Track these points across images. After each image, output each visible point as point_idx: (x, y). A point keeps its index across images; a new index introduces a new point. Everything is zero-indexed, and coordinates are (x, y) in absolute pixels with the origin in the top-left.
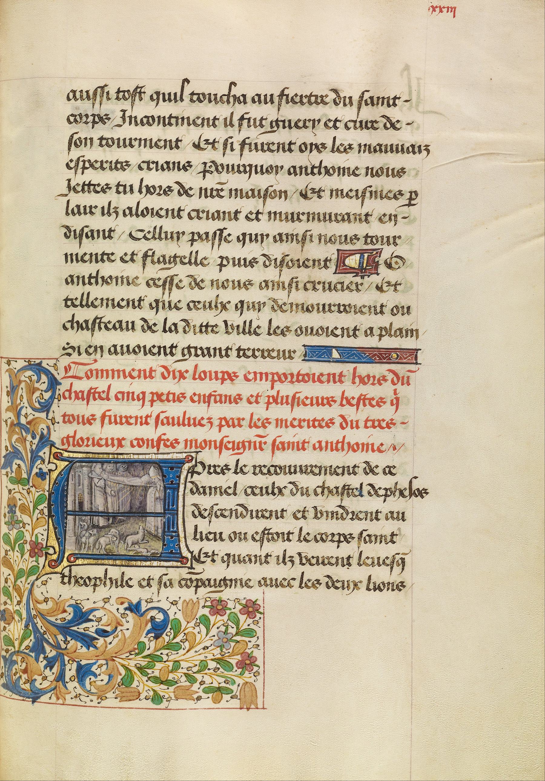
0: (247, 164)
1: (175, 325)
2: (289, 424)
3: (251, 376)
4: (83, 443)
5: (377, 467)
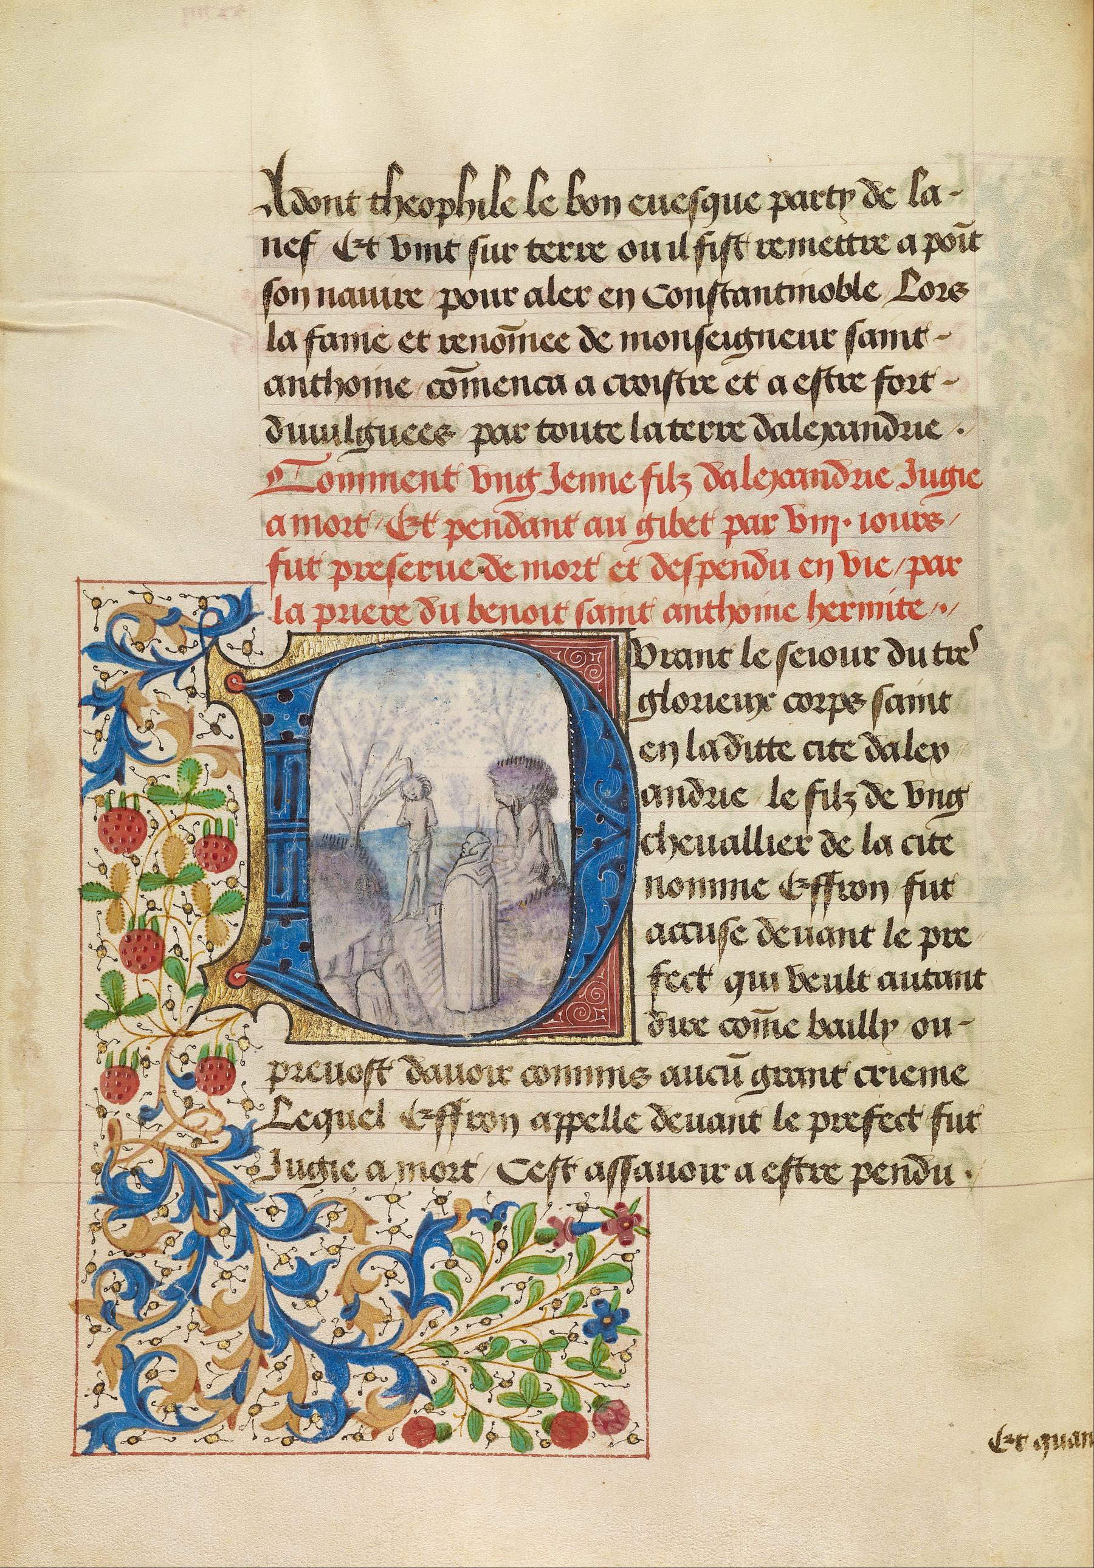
4: (810, 704)
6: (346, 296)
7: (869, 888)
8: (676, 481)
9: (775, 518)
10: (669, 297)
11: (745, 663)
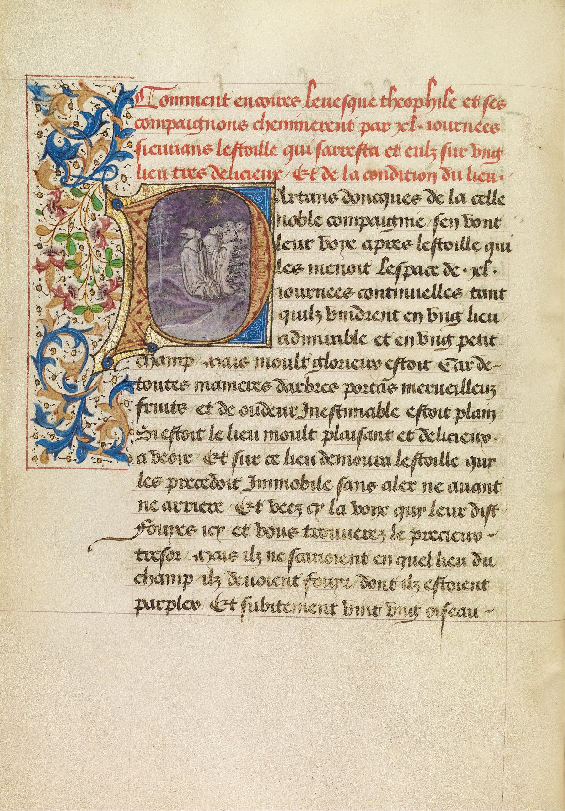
0: (477, 299)
1: (343, 507)
2: (433, 488)
3: (402, 341)
5: (489, 363)
7: (427, 176)
8: (430, 152)
9: (466, 150)
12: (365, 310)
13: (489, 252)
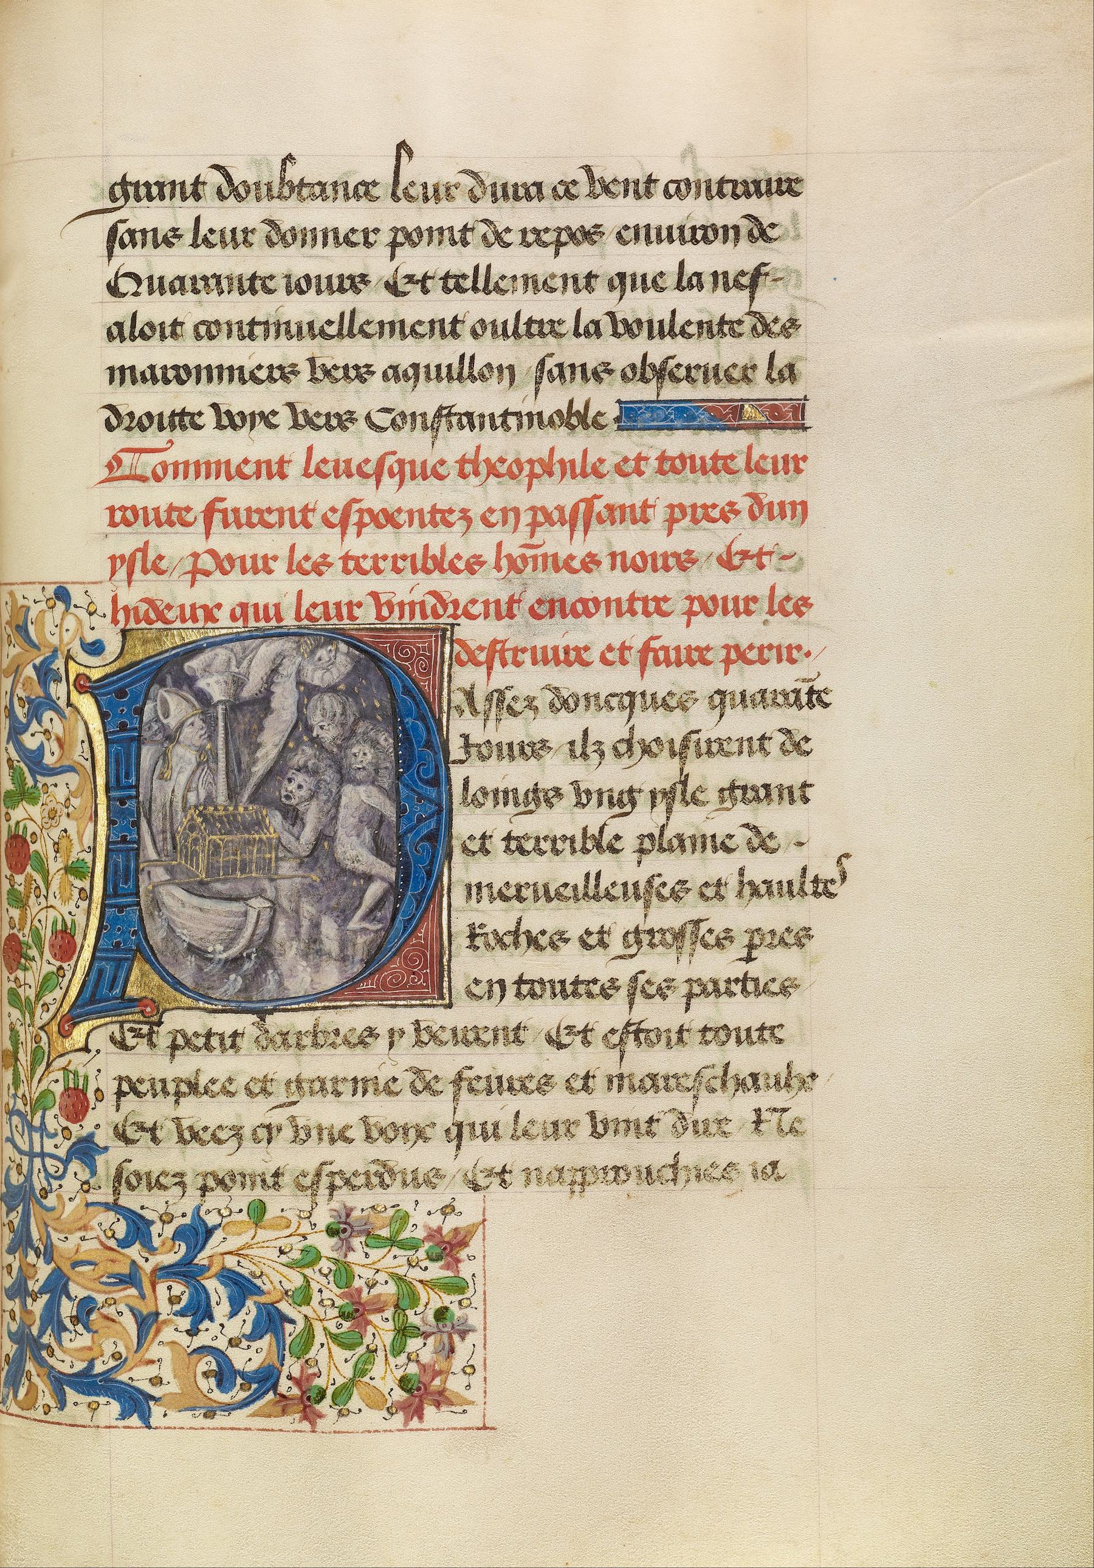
1: (597, 323)
6: (177, 284)
10: (394, 420)
11: (307, 474)
12: (123, 411)
13: (397, 478)
